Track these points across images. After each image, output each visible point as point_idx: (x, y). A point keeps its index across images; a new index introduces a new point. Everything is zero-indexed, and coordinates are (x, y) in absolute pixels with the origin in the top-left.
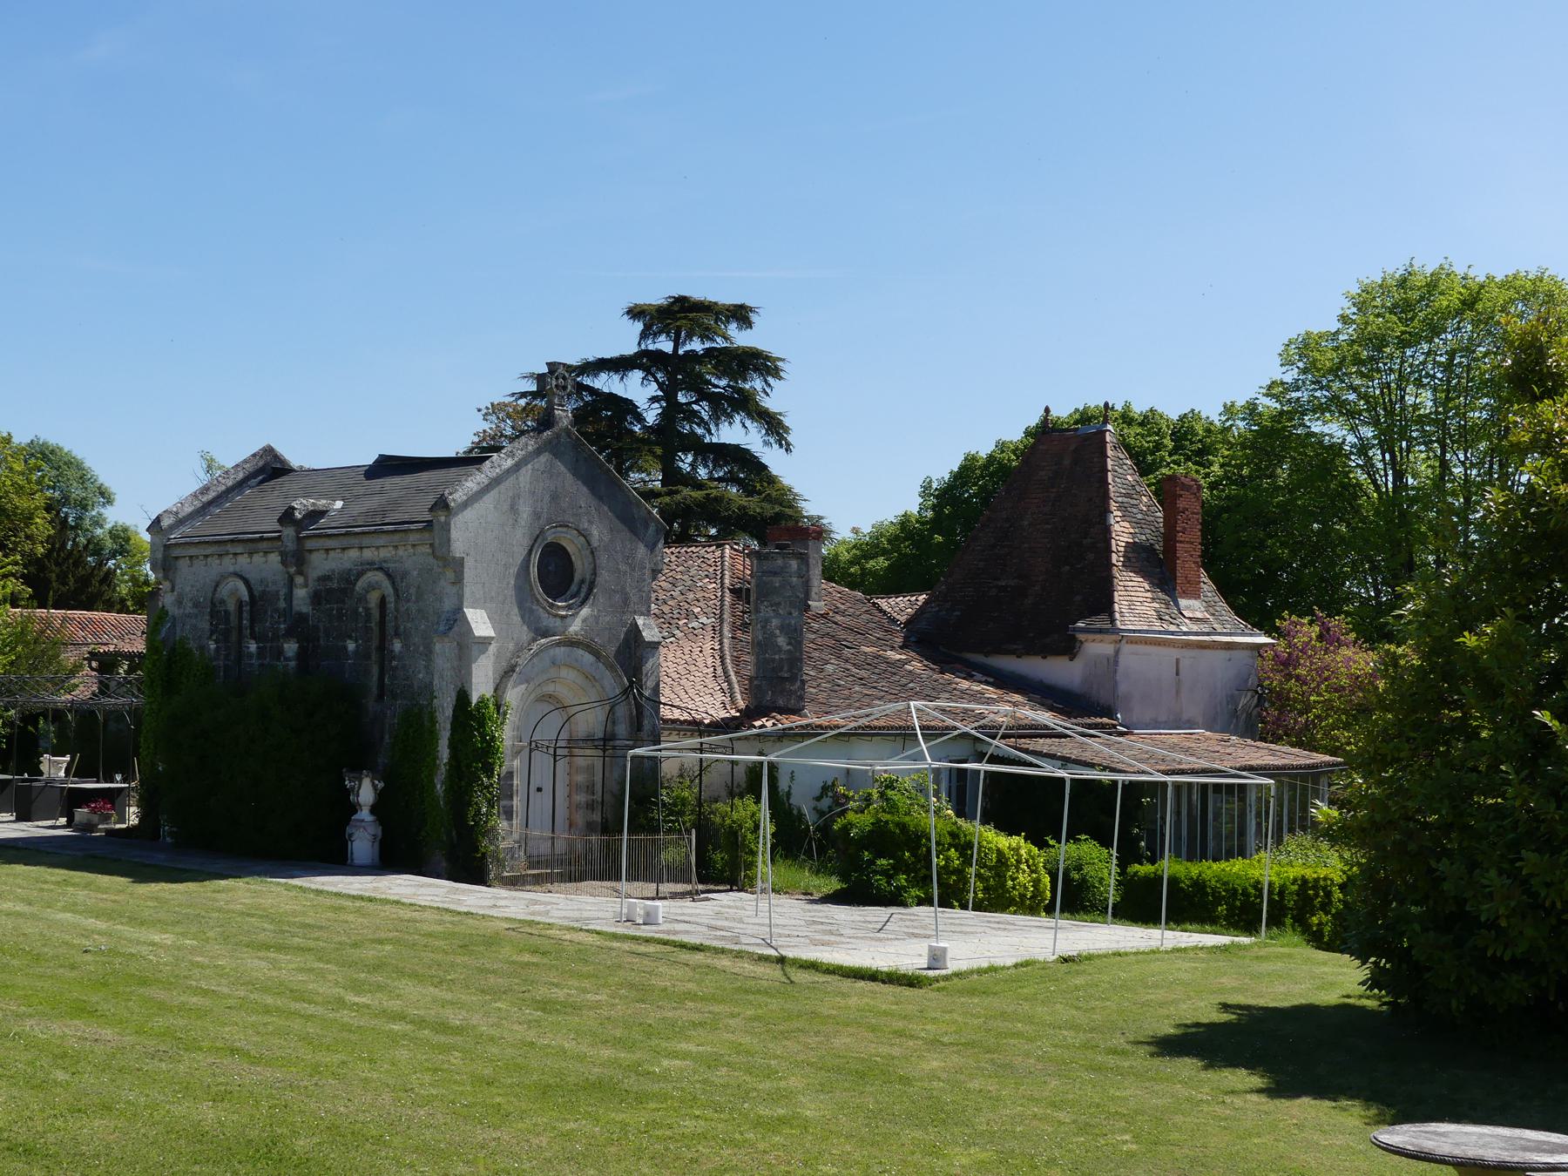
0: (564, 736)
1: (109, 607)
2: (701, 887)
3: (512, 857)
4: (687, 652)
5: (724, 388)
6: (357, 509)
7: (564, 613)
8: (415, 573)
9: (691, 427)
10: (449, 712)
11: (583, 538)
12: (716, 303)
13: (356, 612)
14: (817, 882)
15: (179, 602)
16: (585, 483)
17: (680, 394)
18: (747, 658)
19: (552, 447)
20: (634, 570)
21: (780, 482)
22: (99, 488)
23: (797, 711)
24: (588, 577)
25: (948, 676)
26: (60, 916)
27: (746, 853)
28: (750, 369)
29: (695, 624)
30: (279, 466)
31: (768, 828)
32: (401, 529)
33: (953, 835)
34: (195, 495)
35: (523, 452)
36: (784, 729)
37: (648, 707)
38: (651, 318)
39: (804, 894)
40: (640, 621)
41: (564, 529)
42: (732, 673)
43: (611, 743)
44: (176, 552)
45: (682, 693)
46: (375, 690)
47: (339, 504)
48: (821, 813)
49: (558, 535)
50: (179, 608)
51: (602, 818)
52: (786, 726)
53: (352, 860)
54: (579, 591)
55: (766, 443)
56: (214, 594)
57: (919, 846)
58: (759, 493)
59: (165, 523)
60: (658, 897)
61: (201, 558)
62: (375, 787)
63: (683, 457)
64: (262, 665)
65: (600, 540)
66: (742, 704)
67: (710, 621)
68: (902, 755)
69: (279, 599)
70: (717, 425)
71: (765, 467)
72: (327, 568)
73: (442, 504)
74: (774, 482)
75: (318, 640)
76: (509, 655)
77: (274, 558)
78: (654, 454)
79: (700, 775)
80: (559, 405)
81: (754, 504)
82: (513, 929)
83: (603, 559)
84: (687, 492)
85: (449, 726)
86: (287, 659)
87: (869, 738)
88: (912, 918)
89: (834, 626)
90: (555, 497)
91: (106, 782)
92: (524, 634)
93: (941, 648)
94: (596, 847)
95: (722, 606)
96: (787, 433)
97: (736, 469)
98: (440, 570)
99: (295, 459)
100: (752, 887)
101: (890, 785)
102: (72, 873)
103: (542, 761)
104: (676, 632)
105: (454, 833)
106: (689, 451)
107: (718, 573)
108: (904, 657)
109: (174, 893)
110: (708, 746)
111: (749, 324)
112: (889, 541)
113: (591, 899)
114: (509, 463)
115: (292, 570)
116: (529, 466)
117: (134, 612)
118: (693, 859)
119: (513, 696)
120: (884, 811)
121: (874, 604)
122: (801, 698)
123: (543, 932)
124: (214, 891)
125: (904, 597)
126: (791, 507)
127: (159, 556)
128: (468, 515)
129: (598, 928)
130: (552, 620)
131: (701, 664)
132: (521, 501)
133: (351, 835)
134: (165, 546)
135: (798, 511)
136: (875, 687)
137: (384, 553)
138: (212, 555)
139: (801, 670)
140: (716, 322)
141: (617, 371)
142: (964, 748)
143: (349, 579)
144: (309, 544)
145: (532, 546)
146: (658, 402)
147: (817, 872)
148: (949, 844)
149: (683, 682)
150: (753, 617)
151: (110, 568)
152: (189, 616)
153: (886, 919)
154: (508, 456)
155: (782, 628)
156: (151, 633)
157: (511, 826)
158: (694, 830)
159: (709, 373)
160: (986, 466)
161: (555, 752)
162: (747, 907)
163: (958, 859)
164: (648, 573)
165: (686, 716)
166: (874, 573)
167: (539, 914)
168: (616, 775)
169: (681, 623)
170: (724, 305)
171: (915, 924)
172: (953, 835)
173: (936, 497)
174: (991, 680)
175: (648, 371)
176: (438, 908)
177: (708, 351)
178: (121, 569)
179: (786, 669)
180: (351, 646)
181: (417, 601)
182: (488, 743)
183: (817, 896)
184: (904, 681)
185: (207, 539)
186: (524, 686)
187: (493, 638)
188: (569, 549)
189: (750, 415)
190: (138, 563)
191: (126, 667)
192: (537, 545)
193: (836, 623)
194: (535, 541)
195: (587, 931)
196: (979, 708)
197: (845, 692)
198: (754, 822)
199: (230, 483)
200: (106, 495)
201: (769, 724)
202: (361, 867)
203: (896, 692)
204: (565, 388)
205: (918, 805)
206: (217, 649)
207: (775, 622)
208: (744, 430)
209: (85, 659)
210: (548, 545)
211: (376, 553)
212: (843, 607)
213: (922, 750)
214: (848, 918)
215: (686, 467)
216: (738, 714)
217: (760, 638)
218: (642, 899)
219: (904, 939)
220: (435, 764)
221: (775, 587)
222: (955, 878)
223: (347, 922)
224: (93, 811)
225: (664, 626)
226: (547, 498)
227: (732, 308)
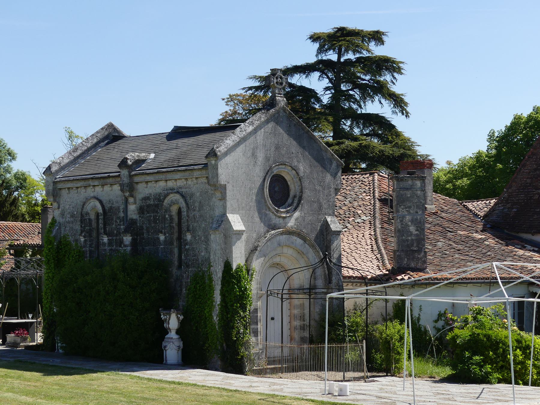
0: (287, 287)
1: (16, 218)
2: (369, 374)
3: (259, 358)
4: (355, 236)
5: (368, 81)
6: (163, 158)
7: (285, 215)
8: (198, 194)
9: (349, 104)
10: (220, 275)
11: (294, 172)
12: (362, 31)
13: (164, 218)
14: (437, 371)
15: (62, 215)
16: (295, 139)
17: (342, 85)
18: (390, 239)
19: (275, 119)
20: (324, 189)
21: (403, 135)
22: (8, 151)
23: (422, 270)
24: (298, 194)
25: (510, 248)
26: (6, 395)
27: (395, 354)
28: (383, 69)
29: (359, 220)
30: (116, 134)
31: (408, 339)
32: (189, 168)
33: (518, 341)
34: (70, 153)
35: (259, 122)
36: (415, 281)
37: (335, 268)
38: (325, 41)
39: (431, 377)
40: (329, 219)
41: (284, 166)
42: (382, 249)
43: (314, 291)
44: (60, 186)
45: (353, 261)
46: (176, 263)
47: (152, 156)
48: (438, 330)
49: (280, 170)
50: (63, 218)
51: (310, 334)
52: (415, 279)
53: (166, 361)
54: (293, 203)
55: (394, 112)
56: (82, 209)
57: (498, 348)
58: (391, 142)
59: (54, 169)
60: (344, 380)
61: (75, 189)
62: (178, 318)
63: (345, 122)
64: (111, 250)
65: (305, 172)
66: (389, 267)
67: (368, 218)
68: (489, 294)
69: (120, 212)
70: (364, 102)
71: (394, 127)
72: (147, 193)
73: (212, 154)
74: (399, 136)
75: (143, 235)
76: (253, 240)
77: (117, 188)
78: (328, 121)
79: (367, 308)
80: (279, 94)
81: (388, 149)
82: (263, 400)
83: (306, 183)
84: (347, 142)
85: (220, 283)
86: (125, 246)
87: (466, 285)
88: (496, 390)
89: (441, 219)
90: (277, 148)
91: (22, 319)
92: (262, 228)
93: (505, 231)
94: (306, 352)
95: (374, 209)
96: (407, 106)
97: (376, 129)
98: (212, 192)
99: (128, 130)
100: (399, 374)
101: (479, 312)
102: (9, 371)
103: (274, 302)
104: (348, 225)
105: (224, 345)
106: (348, 119)
107: (371, 190)
108: (483, 237)
109: (67, 381)
110: (371, 291)
111: (382, 43)
112: (470, 169)
113: (306, 382)
114: (251, 128)
115: (127, 194)
116: (262, 130)
117: (29, 222)
118: (364, 357)
119: (256, 264)
120: (476, 328)
121: (464, 205)
122: (425, 262)
123: (281, 401)
124: (90, 380)
125: (482, 201)
126: (410, 150)
127: (51, 188)
128: (228, 159)
129: (312, 398)
130: (278, 219)
131: (363, 243)
132: (258, 150)
133: (165, 347)
134: (54, 182)
135: (414, 152)
136: (467, 255)
137: (180, 183)
138: (81, 187)
139: (424, 246)
140: (362, 42)
141: (304, 73)
142: (523, 290)
143: (160, 198)
144: (136, 179)
145: (265, 177)
146: (329, 90)
147: (437, 365)
148: (516, 347)
149: (354, 254)
150: (395, 215)
151: (15, 196)
152: (69, 222)
153: (480, 391)
154: (250, 125)
155: (412, 221)
156: (45, 233)
157: (257, 340)
158: (364, 341)
159: (359, 72)
160: (527, 122)
161: (282, 296)
162: (397, 385)
163: (521, 355)
164: (332, 190)
165: (357, 274)
166: (462, 188)
167: (277, 390)
168: (317, 309)
169: (350, 220)
170: (367, 31)
171: (498, 394)
172: (518, 341)
173: (498, 141)
174: (536, 249)
175: (323, 72)
176: (219, 388)
177: (358, 59)
178: (22, 197)
179: (415, 245)
180: (162, 237)
181: (199, 211)
182: (243, 293)
183: (438, 378)
184: (484, 251)
185: (78, 178)
186: (262, 259)
187: (244, 231)
188: (286, 178)
189: (384, 96)
190: (32, 193)
191: (30, 253)
192: (268, 176)
193: (442, 218)
194: (267, 174)
195: (306, 400)
196: (530, 266)
197: (450, 258)
198: (400, 335)
199: (89, 145)
200: (12, 155)
201: (406, 278)
202: (172, 365)
203: (480, 257)
204: (281, 84)
205: (497, 324)
206: (85, 241)
207: (408, 218)
208: (380, 105)
209: (7, 249)
210: (274, 176)
211: (175, 183)
212: (446, 208)
213: (502, 290)
214: (458, 391)
215: (347, 128)
216: (387, 272)
217: (399, 227)
218: (335, 381)
219: (493, 403)
220: (212, 305)
221: (408, 197)
222: (520, 366)
223: (168, 396)
224: (17, 335)
225: (341, 222)
226: (273, 149)
227: (371, 33)
